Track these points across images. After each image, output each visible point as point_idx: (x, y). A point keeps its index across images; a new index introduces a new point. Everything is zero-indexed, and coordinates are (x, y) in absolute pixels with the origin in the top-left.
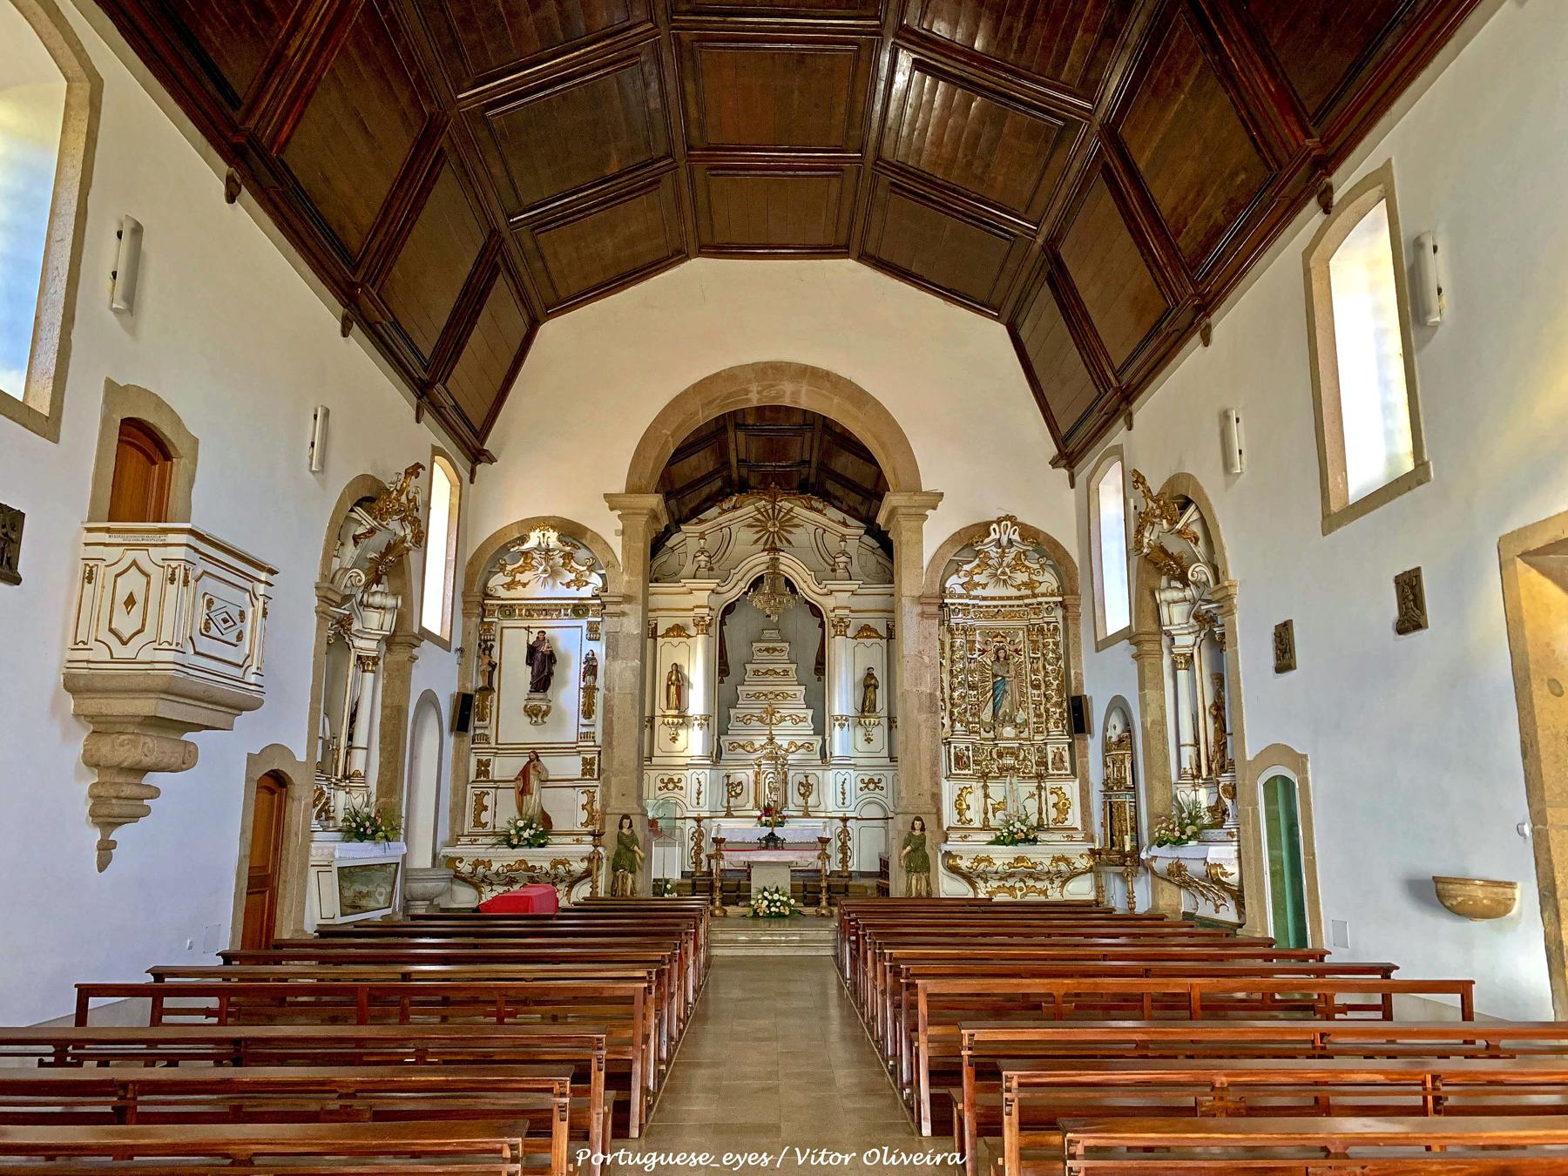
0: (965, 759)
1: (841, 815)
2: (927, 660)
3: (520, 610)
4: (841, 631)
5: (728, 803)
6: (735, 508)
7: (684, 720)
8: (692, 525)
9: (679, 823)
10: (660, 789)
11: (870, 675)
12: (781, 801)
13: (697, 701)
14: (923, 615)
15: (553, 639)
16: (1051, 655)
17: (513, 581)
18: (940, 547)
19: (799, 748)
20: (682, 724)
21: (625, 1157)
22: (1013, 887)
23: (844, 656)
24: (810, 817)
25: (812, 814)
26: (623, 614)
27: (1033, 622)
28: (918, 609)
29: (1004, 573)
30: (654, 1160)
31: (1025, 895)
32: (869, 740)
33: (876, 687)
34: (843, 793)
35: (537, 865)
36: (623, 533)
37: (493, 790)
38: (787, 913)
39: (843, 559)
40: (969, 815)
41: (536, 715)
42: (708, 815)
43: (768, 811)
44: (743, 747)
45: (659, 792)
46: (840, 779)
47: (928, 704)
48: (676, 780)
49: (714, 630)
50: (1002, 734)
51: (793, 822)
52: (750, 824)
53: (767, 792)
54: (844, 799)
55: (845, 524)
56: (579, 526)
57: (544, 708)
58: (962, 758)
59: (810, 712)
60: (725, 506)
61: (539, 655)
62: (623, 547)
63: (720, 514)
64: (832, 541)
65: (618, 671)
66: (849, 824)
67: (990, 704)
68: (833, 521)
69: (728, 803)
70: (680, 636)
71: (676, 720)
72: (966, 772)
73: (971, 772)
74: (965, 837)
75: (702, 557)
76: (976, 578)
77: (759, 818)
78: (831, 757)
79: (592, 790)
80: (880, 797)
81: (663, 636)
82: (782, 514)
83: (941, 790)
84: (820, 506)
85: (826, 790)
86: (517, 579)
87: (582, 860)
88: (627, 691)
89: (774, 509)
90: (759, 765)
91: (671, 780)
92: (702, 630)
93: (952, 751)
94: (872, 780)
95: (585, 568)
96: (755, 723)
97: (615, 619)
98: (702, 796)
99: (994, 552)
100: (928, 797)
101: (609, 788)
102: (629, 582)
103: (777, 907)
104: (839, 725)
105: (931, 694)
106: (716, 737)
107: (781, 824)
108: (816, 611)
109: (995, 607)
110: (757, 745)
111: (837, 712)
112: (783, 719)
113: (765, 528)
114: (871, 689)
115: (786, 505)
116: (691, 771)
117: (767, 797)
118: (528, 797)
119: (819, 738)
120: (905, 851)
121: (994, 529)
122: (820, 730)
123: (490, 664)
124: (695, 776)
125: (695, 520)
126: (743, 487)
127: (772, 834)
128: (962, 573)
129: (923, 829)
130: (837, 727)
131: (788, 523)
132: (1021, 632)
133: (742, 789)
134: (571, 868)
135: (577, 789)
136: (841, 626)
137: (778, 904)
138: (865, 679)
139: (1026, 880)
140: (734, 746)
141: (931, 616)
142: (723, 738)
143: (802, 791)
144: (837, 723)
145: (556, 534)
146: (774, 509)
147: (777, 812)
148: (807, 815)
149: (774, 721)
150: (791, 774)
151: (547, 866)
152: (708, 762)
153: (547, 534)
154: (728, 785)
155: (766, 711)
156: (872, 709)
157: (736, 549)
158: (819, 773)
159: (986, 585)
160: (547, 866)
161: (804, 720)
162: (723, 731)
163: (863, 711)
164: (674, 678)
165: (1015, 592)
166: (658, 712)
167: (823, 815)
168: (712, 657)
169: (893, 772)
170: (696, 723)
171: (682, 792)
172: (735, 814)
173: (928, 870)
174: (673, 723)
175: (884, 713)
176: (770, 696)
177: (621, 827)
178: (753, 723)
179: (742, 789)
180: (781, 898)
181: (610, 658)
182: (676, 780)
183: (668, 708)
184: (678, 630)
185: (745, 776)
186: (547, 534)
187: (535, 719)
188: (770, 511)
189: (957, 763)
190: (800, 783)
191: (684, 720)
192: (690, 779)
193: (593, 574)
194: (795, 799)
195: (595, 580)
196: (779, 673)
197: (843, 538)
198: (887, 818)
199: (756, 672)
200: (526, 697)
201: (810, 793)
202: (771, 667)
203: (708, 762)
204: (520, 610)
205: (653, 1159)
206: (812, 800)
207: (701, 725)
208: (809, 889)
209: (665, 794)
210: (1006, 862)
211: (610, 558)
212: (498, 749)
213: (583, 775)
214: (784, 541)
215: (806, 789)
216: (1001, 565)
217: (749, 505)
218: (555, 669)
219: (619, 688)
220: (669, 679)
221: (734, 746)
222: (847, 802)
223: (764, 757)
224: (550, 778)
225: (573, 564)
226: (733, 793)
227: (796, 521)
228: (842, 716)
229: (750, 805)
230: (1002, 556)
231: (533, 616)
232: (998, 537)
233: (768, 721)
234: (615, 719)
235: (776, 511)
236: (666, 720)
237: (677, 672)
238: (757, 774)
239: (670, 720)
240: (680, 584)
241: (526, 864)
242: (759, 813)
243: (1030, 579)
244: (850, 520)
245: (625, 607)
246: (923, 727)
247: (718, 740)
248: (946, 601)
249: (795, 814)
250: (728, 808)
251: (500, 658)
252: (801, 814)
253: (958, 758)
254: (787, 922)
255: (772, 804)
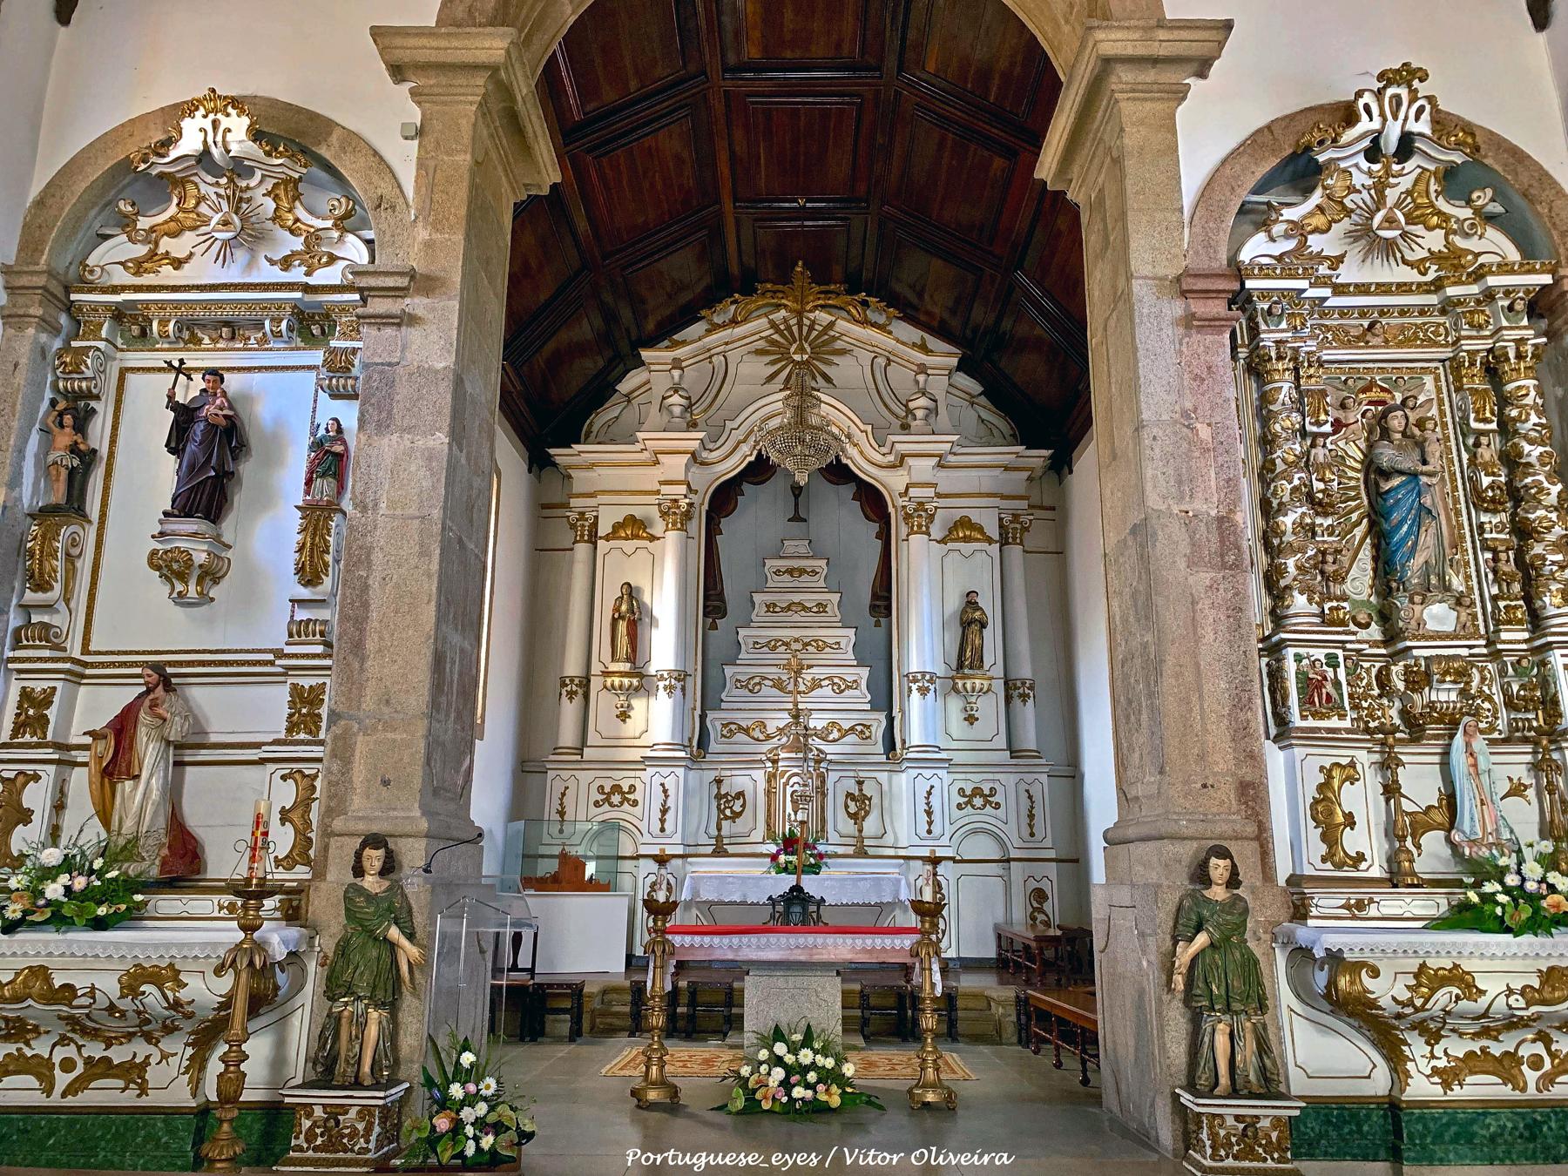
0: (1329, 688)
1: (926, 852)
2: (1204, 432)
3: (164, 322)
4: (920, 526)
5: (719, 829)
6: (734, 322)
7: (641, 682)
8: (660, 350)
9: (627, 865)
10: (597, 804)
11: (970, 602)
12: (813, 825)
13: (663, 650)
14: (1189, 322)
15: (247, 398)
16: (1534, 419)
17: (152, 255)
18: (1224, 162)
19: (844, 733)
20: (637, 689)
21: (675, 1157)
22: (1512, 1057)
23: (926, 569)
24: (865, 855)
25: (871, 851)
26: (407, 320)
27: (1467, 345)
28: (1177, 308)
29: (1390, 222)
30: (703, 1160)
31: (1548, 1080)
32: (971, 719)
33: (983, 625)
34: (929, 813)
35: (81, 982)
36: (420, 133)
37: (51, 769)
38: (835, 1101)
39: (923, 402)
40: (1352, 841)
41: (183, 577)
42: (679, 850)
43: (790, 844)
44: (746, 731)
45: (594, 810)
46: (922, 787)
47: (1215, 545)
48: (626, 789)
49: (698, 526)
50: (1420, 623)
51: (835, 866)
52: (759, 868)
53: (789, 809)
54: (930, 823)
55: (923, 348)
56: (313, 117)
57: (200, 558)
58: (1320, 686)
59: (864, 673)
60: (717, 319)
61: (199, 428)
62: (421, 164)
63: (709, 332)
64: (901, 377)
65: (388, 459)
66: (940, 869)
67: (1366, 554)
68: (903, 343)
69: (719, 829)
70: (637, 537)
71: (626, 681)
72: (1334, 722)
73: (1347, 724)
74: (1360, 905)
75: (676, 399)
76: (1315, 243)
77: (774, 857)
78: (903, 748)
79: (309, 769)
80: (993, 821)
81: (607, 538)
82: (815, 333)
83: (1264, 775)
84: (882, 320)
85: (895, 807)
86: (161, 250)
87: (219, 971)
88: (413, 511)
89: (800, 325)
90: (775, 762)
91: (617, 788)
92: (674, 524)
93: (1291, 667)
94: (977, 791)
95: (329, 224)
96: (767, 690)
97: (389, 331)
98: (670, 816)
99: (1361, 172)
100: (1227, 793)
101: (347, 762)
102: (429, 245)
103: (808, 1086)
104: (919, 689)
105: (1220, 520)
106: (698, 712)
107: (814, 869)
108: (872, 501)
109: (1363, 312)
110: (771, 729)
111: (914, 666)
112: (816, 684)
113: (785, 356)
114: (975, 627)
115: (823, 317)
116: (651, 771)
117: (790, 818)
118: (128, 784)
119: (882, 716)
120: (1185, 953)
121: (1367, 108)
122: (884, 698)
123: (74, 449)
124: (657, 780)
125: (666, 343)
126: (745, 284)
127: (797, 888)
128: (1278, 229)
129: (1233, 881)
130: (915, 695)
131: (825, 347)
132: (1429, 380)
133: (743, 806)
134: (183, 995)
135: (271, 767)
136: (920, 517)
137: (812, 1077)
138: (964, 611)
139: (1555, 1035)
140: (731, 729)
141: (1211, 324)
142: (711, 715)
143: (853, 809)
144: (914, 687)
145: (246, 121)
146: (800, 325)
147: (807, 846)
148: (861, 853)
149: (802, 688)
150: (832, 778)
151: (109, 986)
152: (682, 754)
153: (225, 122)
154: (719, 797)
155: (787, 667)
156: (976, 663)
157: (734, 392)
158: (883, 777)
159: (1340, 259)
160: (109, 986)
161: (854, 685)
162: (709, 700)
163: (960, 666)
164: (624, 608)
165: (1412, 276)
166: (596, 668)
167: (891, 852)
168: (692, 561)
169: (1017, 777)
170: (661, 684)
171: (637, 810)
172: (731, 849)
173: (1262, 1007)
174: (621, 687)
175: (998, 671)
176: (795, 646)
177: (359, 871)
178: (766, 691)
179: (743, 806)
180: (820, 1060)
181: (371, 428)
182: (626, 789)
183: (614, 659)
184: (634, 527)
185: (751, 781)
186: (225, 122)
187: (179, 587)
188: (795, 329)
189: (1306, 701)
190: (849, 795)
191: (641, 682)
192: (648, 783)
193: (350, 238)
194: (840, 824)
195: (354, 250)
196: (810, 609)
197: (922, 369)
198: (1008, 861)
199: (771, 607)
200: (157, 529)
201: (867, 813)
202: (796, 598)
203: (682, 754)
204: (164, 322)
205: (703, 1159)
206: (871, 825)
207: (670, 689)
208: (873, 1001)
209: (607, 813)
210: (1517, 985)
211: (385, 188)
212: (86, 665)
213: (289, 730)
214: (819, 378)
215: (859, 806)
216: (1380, 201)
217: (759, 317)
218: (247, 469)
219: (392, 504)
220: (617, 609)
221: (731, 729)
222: (936, 829)
223: (783, 747)
224: (213, 738)
225: (300, 212)
226: (728, 812)
227: (839, 345)
228: (924, 674)
229: (758, 834)
230: (1380, 187)
231: (200, 341)
232: (1376, 124)
233: (791, 687)
234: (375, 583)
235: (805, 329)
236: (609, 680)
237: (630, 595)
238: (771, 778)
239: (617, 681)
240: (638, 446)
241: (48, 979)
242: (773, 849)
243: (1448, 244)
244: (933, 342)
245: (415, 304)
246: (1204, 605)
247: (703, 717)
248: (1249, 284)
249: (840, 850)
250: (719, 838)
251: (113, 442)
252: (850, 850)
253: (1310, 686)
254: (836, 1126)
255: (798, 831)
